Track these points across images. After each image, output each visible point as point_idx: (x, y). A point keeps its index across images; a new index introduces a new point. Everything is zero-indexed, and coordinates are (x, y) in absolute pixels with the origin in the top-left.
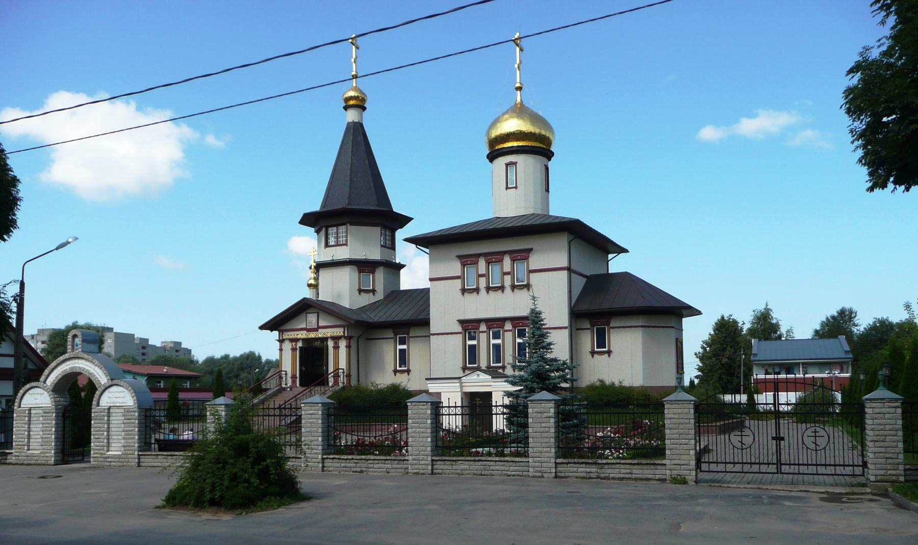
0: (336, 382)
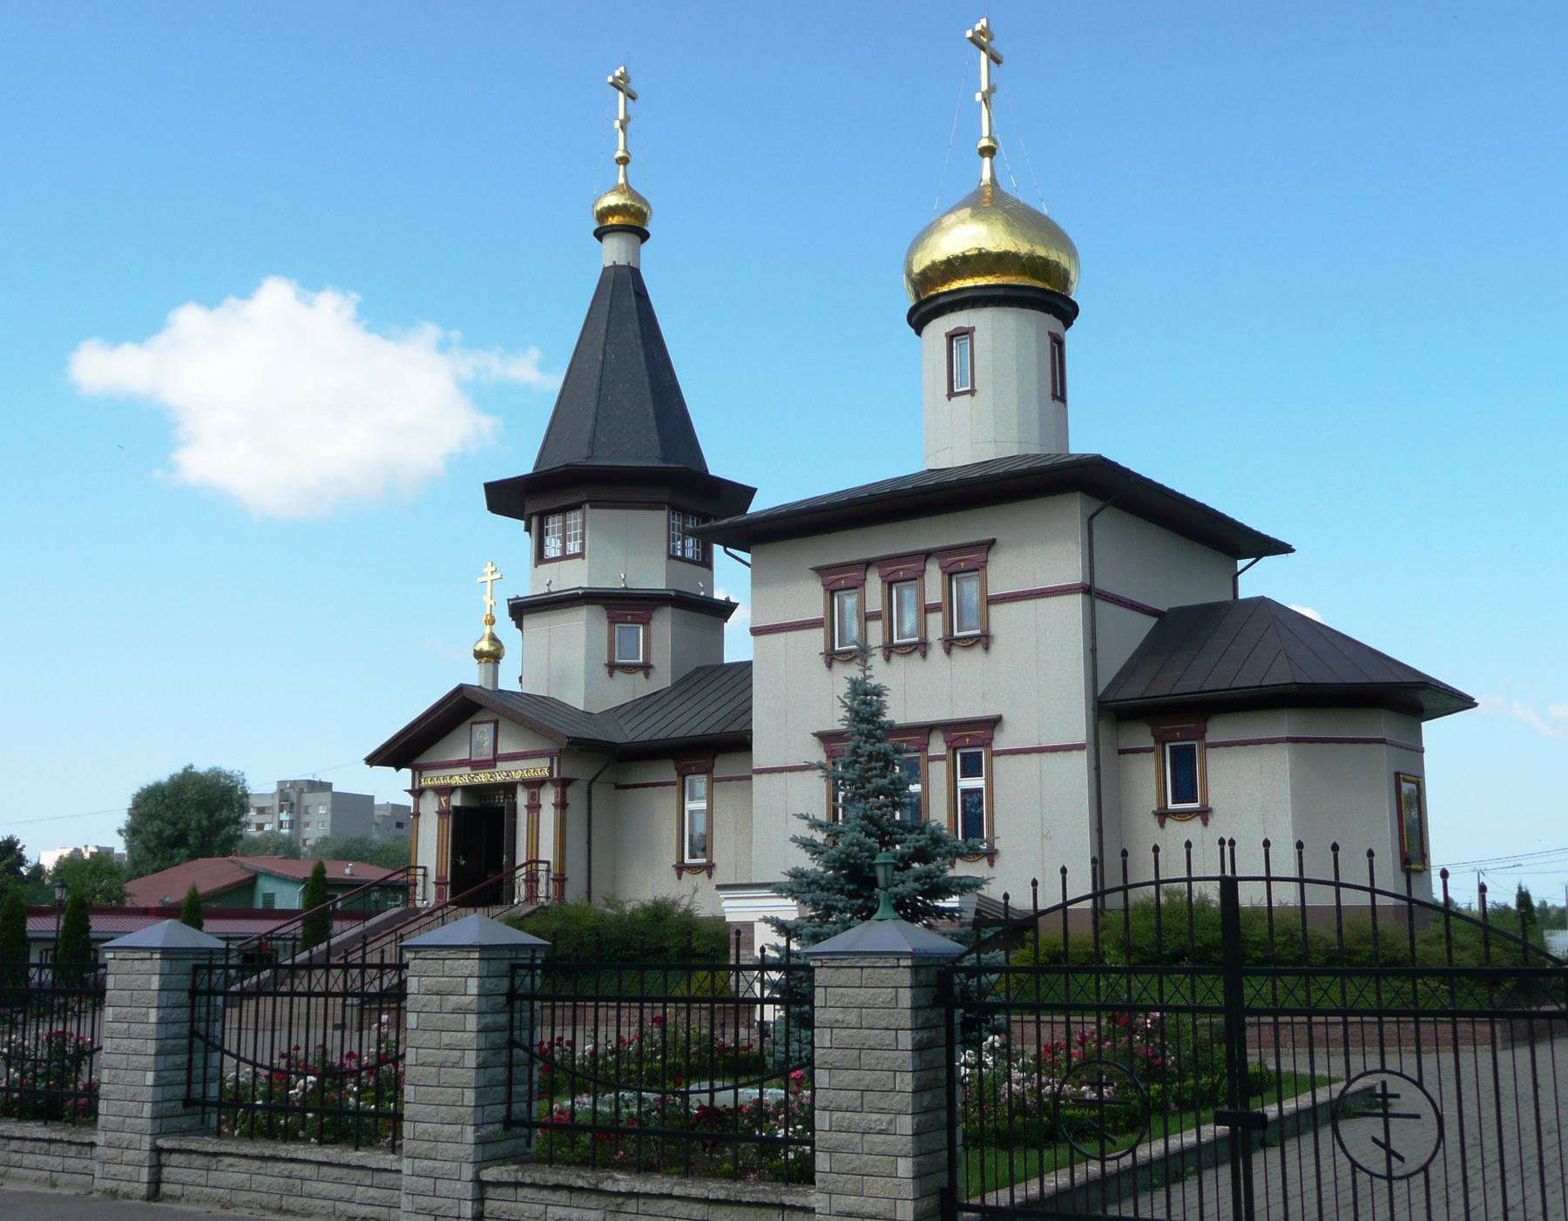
0: (532, 895)
